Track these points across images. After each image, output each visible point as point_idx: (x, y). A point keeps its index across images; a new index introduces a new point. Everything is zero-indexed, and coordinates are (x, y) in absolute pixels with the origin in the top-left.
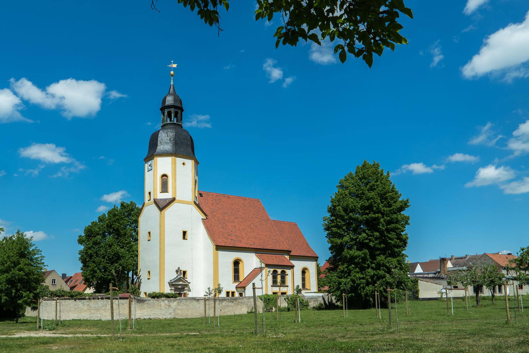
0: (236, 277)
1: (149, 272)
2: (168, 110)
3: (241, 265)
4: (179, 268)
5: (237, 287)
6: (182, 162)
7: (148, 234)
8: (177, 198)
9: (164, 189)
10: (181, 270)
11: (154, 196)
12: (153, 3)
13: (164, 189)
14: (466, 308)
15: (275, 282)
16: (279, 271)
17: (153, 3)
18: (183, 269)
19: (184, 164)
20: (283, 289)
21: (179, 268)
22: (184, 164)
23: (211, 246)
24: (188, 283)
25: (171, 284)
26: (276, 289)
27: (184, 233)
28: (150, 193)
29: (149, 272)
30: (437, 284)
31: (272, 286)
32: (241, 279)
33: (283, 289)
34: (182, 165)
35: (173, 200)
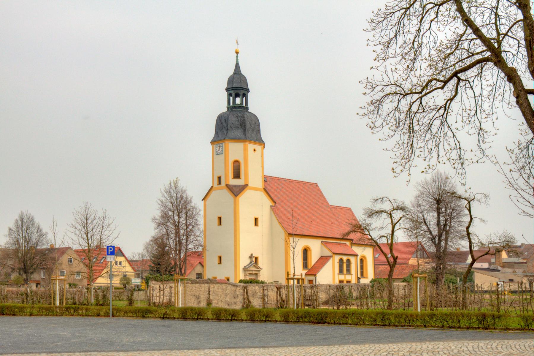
0: (305, 265)
1: (446, 33)
2: (236, 92)
3: (309, 252)
5: (307, 275)
6: (253, 149)
7: (217, 260)
8: (250, 185)
9: (237, 174)
11: (226, 182)
12: (431, 33)
13: (237, 174)
15: (341, 271)
16: (345, 258)
17: (431, 33)
18: (255, 255)
19: (255, 150)
20: (348, 278)
21: (252, 255)
22: (255, 150)
23: (281, 234)
24: (260, 270)
25: (245, 269)
26: (342, 277)
27: (256, 219)
29: (446, 33)
30: (492, 276)
31: (338, 274)
32: (310, 267)
33: (348, 278)
34: (253, 151)
35: (246, 186)
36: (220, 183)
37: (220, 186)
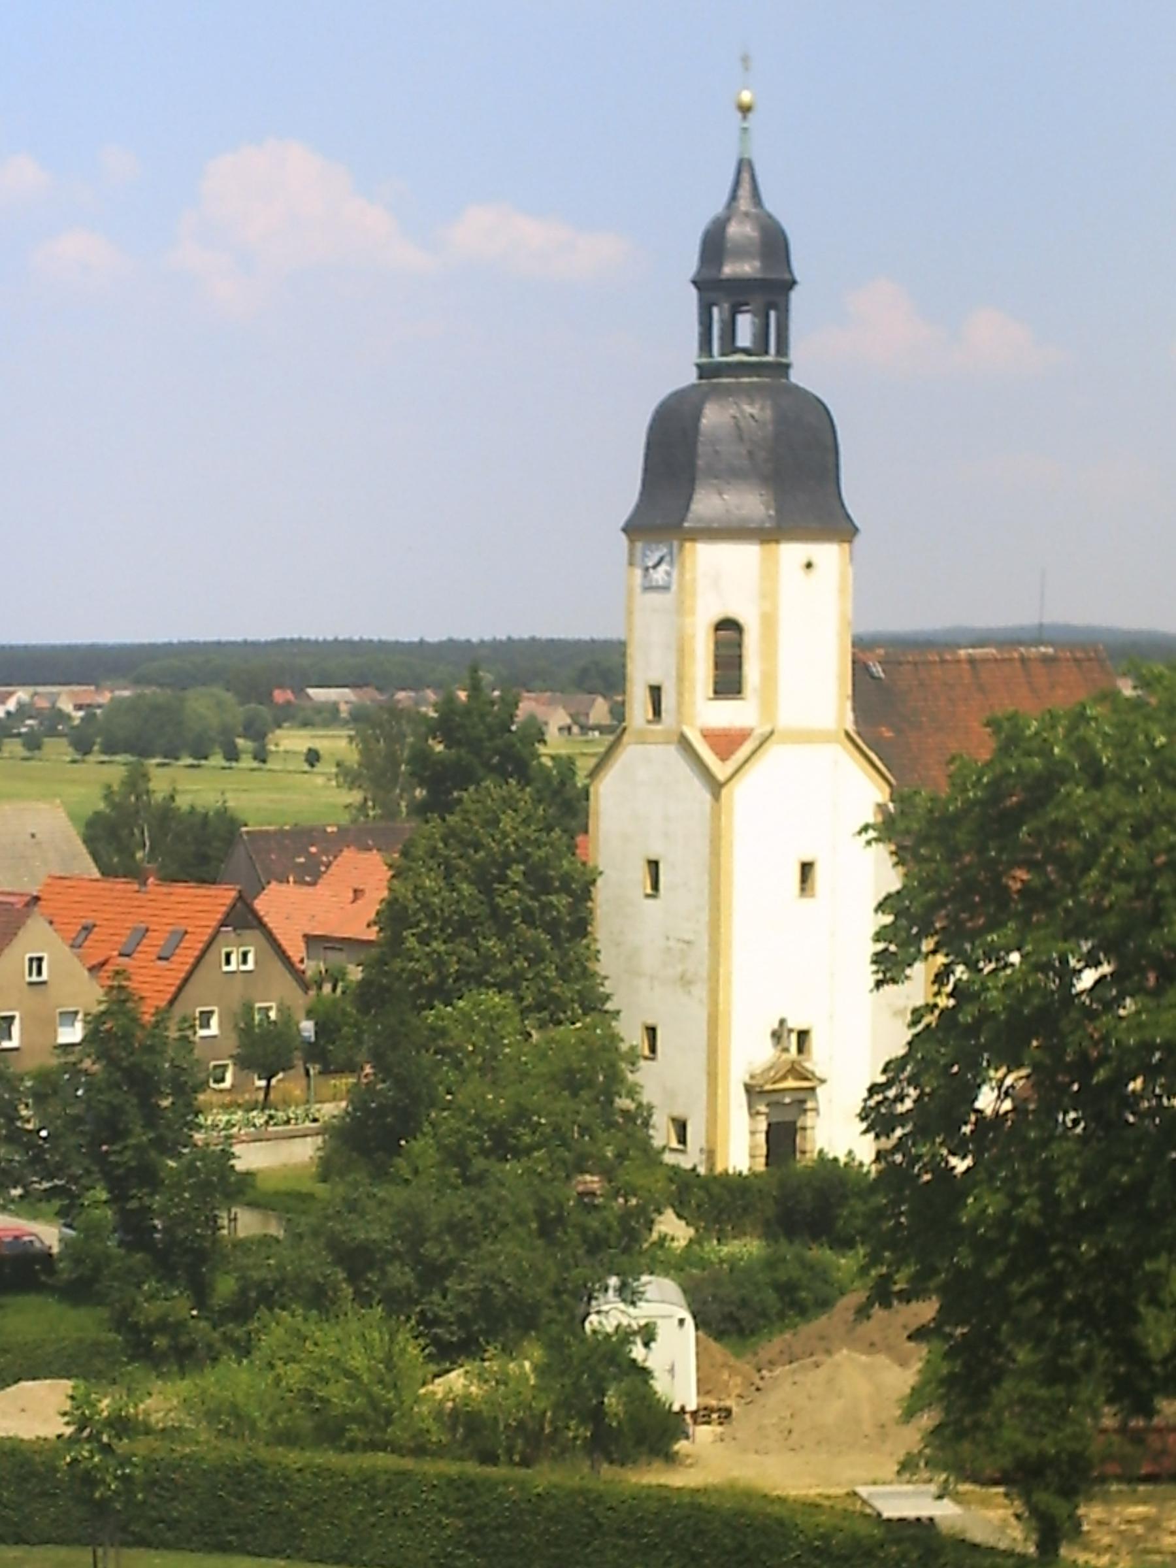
4: (782, 1022)
10: (791, 1031)
14: (801, 1095)
18: (796, 1023)
28: (656, 692)
34: (805, 561)
36: (657, 711)
37: (658, 727)
